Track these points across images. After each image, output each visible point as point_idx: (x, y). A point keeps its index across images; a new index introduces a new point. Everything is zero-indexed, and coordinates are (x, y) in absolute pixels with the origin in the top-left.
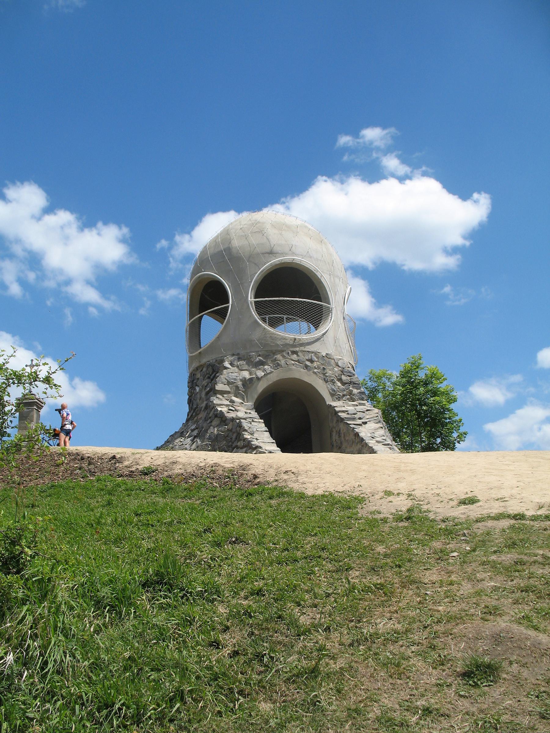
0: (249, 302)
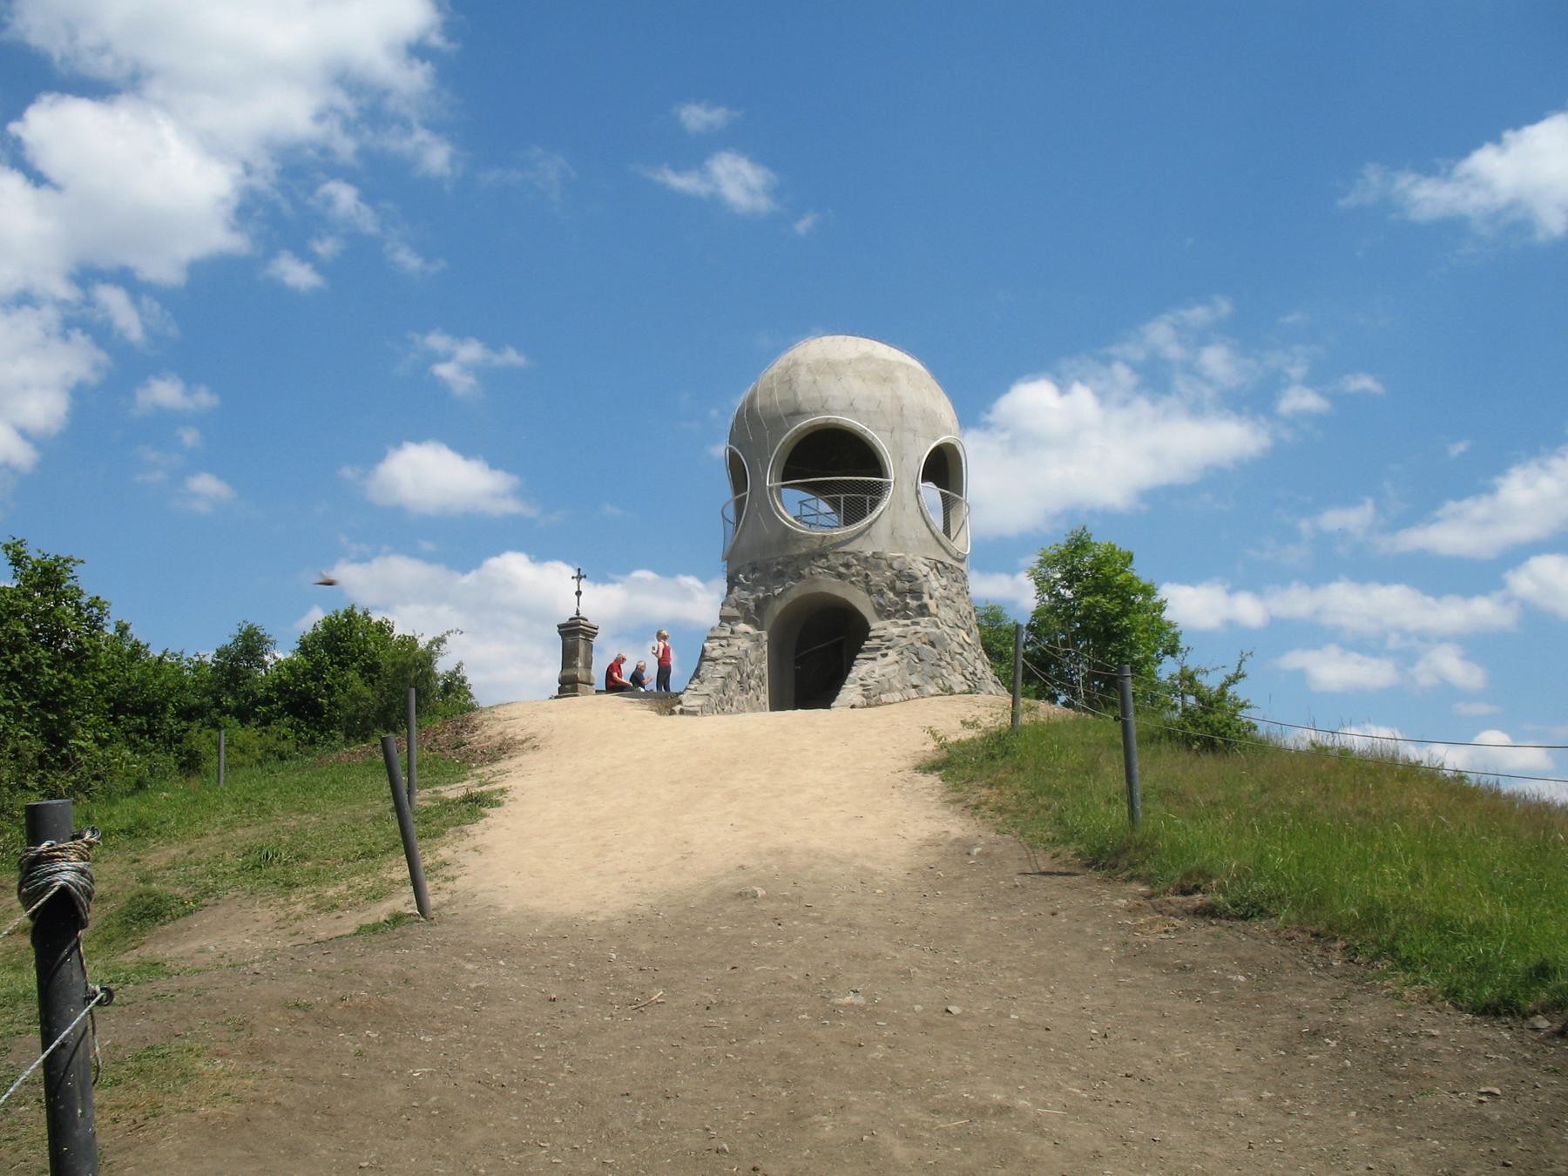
0: (767, 489)
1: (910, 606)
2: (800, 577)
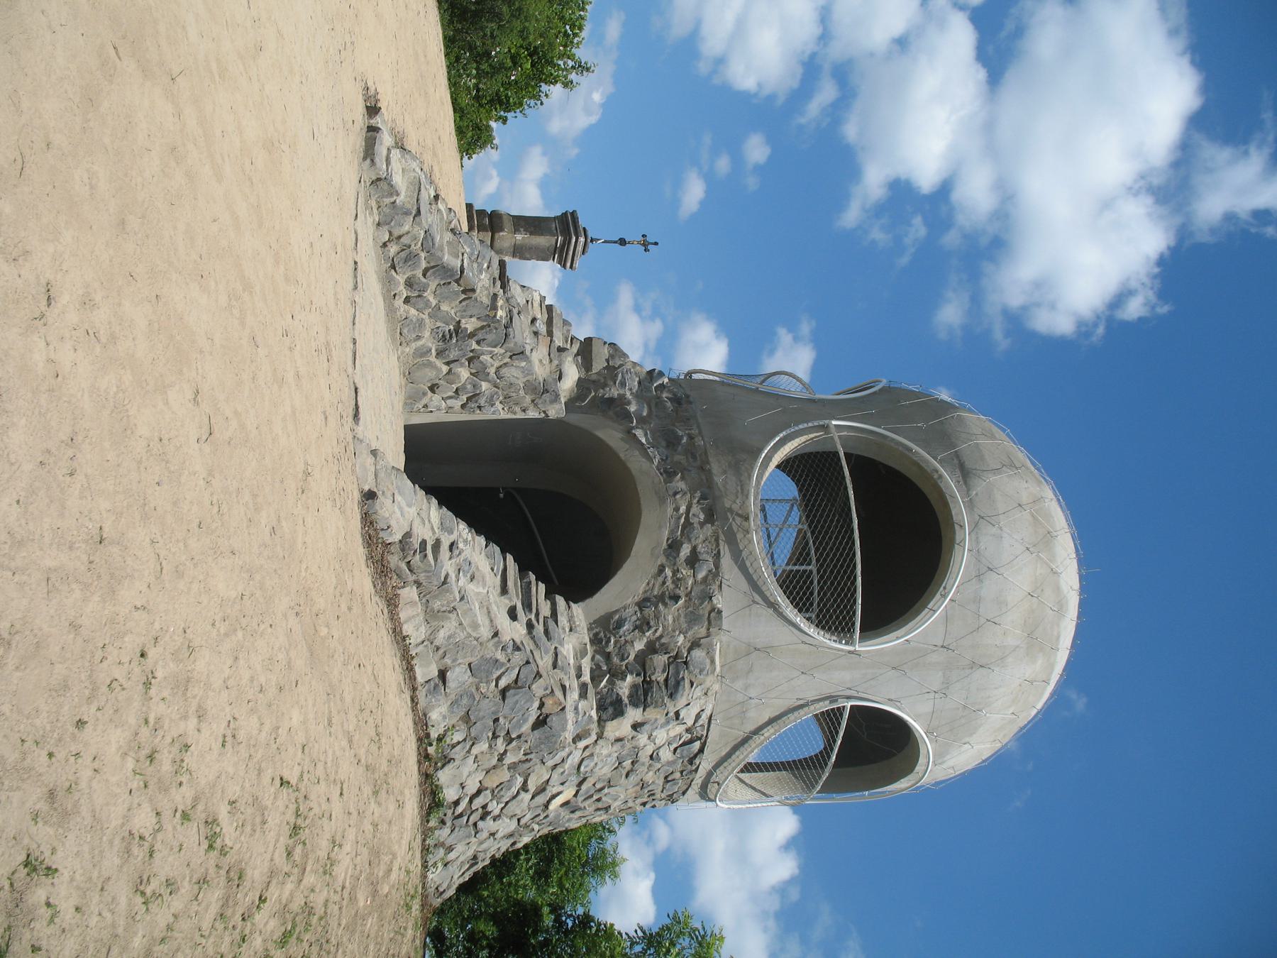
0: (827, 422)
2: (669, 475)
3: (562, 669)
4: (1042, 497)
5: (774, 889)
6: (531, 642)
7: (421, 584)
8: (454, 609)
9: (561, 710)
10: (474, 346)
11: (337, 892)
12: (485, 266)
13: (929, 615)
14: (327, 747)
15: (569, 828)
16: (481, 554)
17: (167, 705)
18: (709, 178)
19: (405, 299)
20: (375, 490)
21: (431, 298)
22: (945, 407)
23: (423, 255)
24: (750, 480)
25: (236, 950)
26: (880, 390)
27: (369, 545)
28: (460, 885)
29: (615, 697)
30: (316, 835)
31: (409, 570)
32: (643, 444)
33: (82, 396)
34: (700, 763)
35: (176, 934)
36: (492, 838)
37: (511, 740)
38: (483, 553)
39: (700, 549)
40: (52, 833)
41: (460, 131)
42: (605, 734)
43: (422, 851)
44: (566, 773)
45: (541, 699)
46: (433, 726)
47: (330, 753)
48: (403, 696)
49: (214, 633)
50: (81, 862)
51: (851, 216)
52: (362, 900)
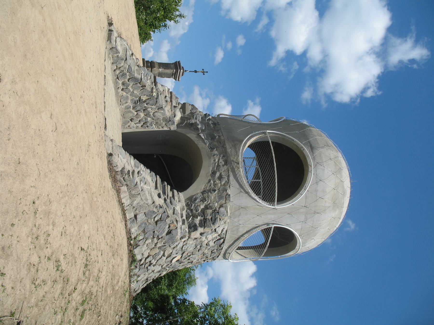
0: (265, 131)
1: (195, 219)
2: (212, 149)
3: (176, 214)
4: (338, 156)
5: (248, 290)
6: (166, 205)
7: (128, 185)
8: (139, 194)
9: (176, 228)
10: (146, 105)
11: (101, 288)
12: (149, 78)
13: (300, 196)
14: (97, 239)
15: (179, 269)
16: (148, 175)
17: (42, 220)
18: (225, 50)
19: (122, 89)
20: (112, 153)
21: (131, 89)
22: (305, 126)
23: (128, 74)
24: (239, 151)
25: (67, 306)
26: (283, 120)
27: (110, 172)
28: (142, 289)
29: (194, 224)
30: (93, 268)
31: (124, 180)
32: (203, 139)
33: (12, 114)
34: (223, 246)
35: (46, 299)
36: (153, 272)
37: (159, 239)
38: (149, 175)
39: (223, 174)
40: (3, 262)
41: (140, 34)
42: (191, 237)
43: (129, 277)
44: (178, 250)
45: (169, 225)
46: (132, 234)
47: (98, 240)
48: (122, 223)
49: (58, 197)
50: (13, 272)
51: (273, 62)
52: (109, 291)
